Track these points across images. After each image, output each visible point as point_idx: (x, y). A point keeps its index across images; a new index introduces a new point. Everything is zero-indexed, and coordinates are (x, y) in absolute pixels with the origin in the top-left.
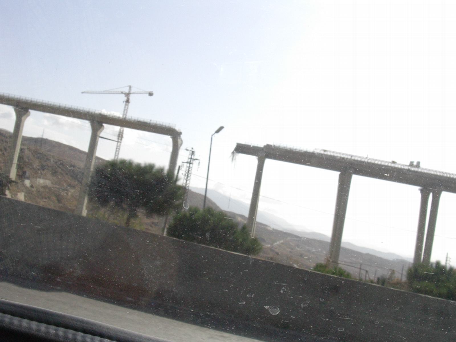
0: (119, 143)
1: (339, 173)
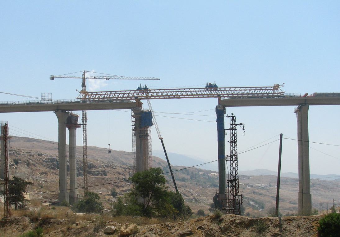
0: (84, 126)
1: (309, 106)
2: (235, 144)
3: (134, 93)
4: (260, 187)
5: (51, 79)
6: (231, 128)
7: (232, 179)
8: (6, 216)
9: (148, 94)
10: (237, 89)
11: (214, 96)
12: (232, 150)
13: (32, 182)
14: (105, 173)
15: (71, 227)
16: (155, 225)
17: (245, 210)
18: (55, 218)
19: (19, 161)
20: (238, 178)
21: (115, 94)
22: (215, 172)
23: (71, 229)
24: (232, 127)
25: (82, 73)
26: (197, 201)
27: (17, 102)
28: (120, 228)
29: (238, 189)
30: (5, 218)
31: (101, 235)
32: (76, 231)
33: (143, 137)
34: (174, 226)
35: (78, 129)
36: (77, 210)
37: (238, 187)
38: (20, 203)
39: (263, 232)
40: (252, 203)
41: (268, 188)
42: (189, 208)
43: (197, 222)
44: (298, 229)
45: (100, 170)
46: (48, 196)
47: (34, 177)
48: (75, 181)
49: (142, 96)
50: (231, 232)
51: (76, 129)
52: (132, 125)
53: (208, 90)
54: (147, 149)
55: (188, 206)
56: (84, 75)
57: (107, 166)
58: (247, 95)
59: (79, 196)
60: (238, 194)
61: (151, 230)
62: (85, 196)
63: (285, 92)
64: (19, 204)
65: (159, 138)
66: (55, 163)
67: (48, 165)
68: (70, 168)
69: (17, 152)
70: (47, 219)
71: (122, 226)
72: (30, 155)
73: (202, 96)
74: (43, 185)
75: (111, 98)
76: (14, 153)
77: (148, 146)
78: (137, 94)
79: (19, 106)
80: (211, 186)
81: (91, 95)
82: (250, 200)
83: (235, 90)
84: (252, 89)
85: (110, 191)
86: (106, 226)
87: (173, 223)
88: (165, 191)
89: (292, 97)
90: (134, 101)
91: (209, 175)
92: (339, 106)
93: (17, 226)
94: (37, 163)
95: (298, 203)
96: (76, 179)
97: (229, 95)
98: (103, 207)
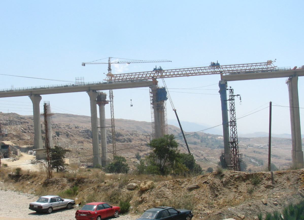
0: (112, 102)
2: (233, 112)
3: (151, 74)
4: (259, 147)
5: (83, 65)
6: (230, 99)
7: (232, 141)
8: (49, 178)
9: (162, 74)
10: (236, 66)
11: (217, 73)
12: (231, 117)
13: (71, 150)
14: (130, 140)
15: (100, 185)
16: (168, 181)
17: (247, 167)
18: (88, 178)
19: (60, 133)
20: (237, 140)
21: (135, 75)
22: (221, 136)
23: (101, 186)
24: (230, 98)
25: (108, 59)
26: (207, 160)
27: (56, 86)
28: (139, 185)
29: (238, 149)
30: (47, 179)
31: (124, 191)
32: (105, 188)
33: (160, 109)
34: (184, 182)
35: (106, 105)
36: (108, 171)
37: (237, 147)
38: (61, 167)
39: (258, 185)
40: (253, 161)
41: (266, 148)
42: (200, 167)
43: (203, 178)
44: (287, 181)
45: (126, 137)
46: (84, 161)
47: (73, 145)
48: (105, 147)
49: (158, 76)
50: (231, 185)
51: (105, 105)
52: (151, 100)
53: (212, 68)
54: (164, 119)
55: (199, 164)
56: (110, 60)
57: (132, 135)
58: (244, 71)
59: (110, 160)
60: (238, 153)
61: (165, 186)
62: (114, 159)
63: (277, 66)
64: (60, 168)
65: (173, 110)
66: (89, 133)
67: (83, 135)
68: (101, 137)
69: (58, 126)
70: (81, 179)
71: (141, 183)
72: (69, 128)
73: (207, 73)
74: (80, 152)
75: (132, 78)
76: (55, 127)
77: (164, 117)
78: (153, 74)
79: (42, 89)
80: (218, 147)
81: (116, 77)
82: (251, 158)
83: (235, 67)
84: (249, 65)
85: (135, 155)
86: (128, 183)
87: (183, 179)
88: (178, 154)
89: (283, 70)
90: (151, 80)
91: (216, 138)
92: (303, 77)
93: (58, 186)
94: (75, 134)
95: (292, 159)
96: (106, 146)
97: (230, 72)
98: (129, 168)
